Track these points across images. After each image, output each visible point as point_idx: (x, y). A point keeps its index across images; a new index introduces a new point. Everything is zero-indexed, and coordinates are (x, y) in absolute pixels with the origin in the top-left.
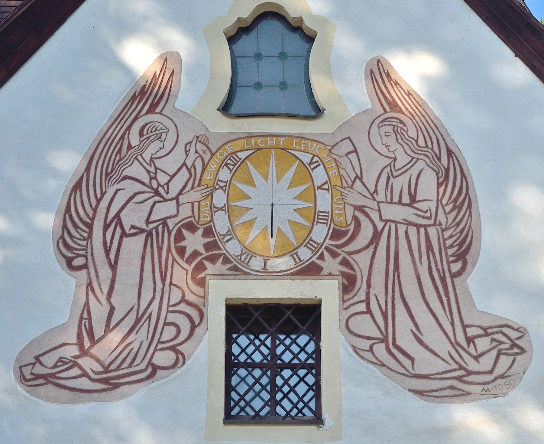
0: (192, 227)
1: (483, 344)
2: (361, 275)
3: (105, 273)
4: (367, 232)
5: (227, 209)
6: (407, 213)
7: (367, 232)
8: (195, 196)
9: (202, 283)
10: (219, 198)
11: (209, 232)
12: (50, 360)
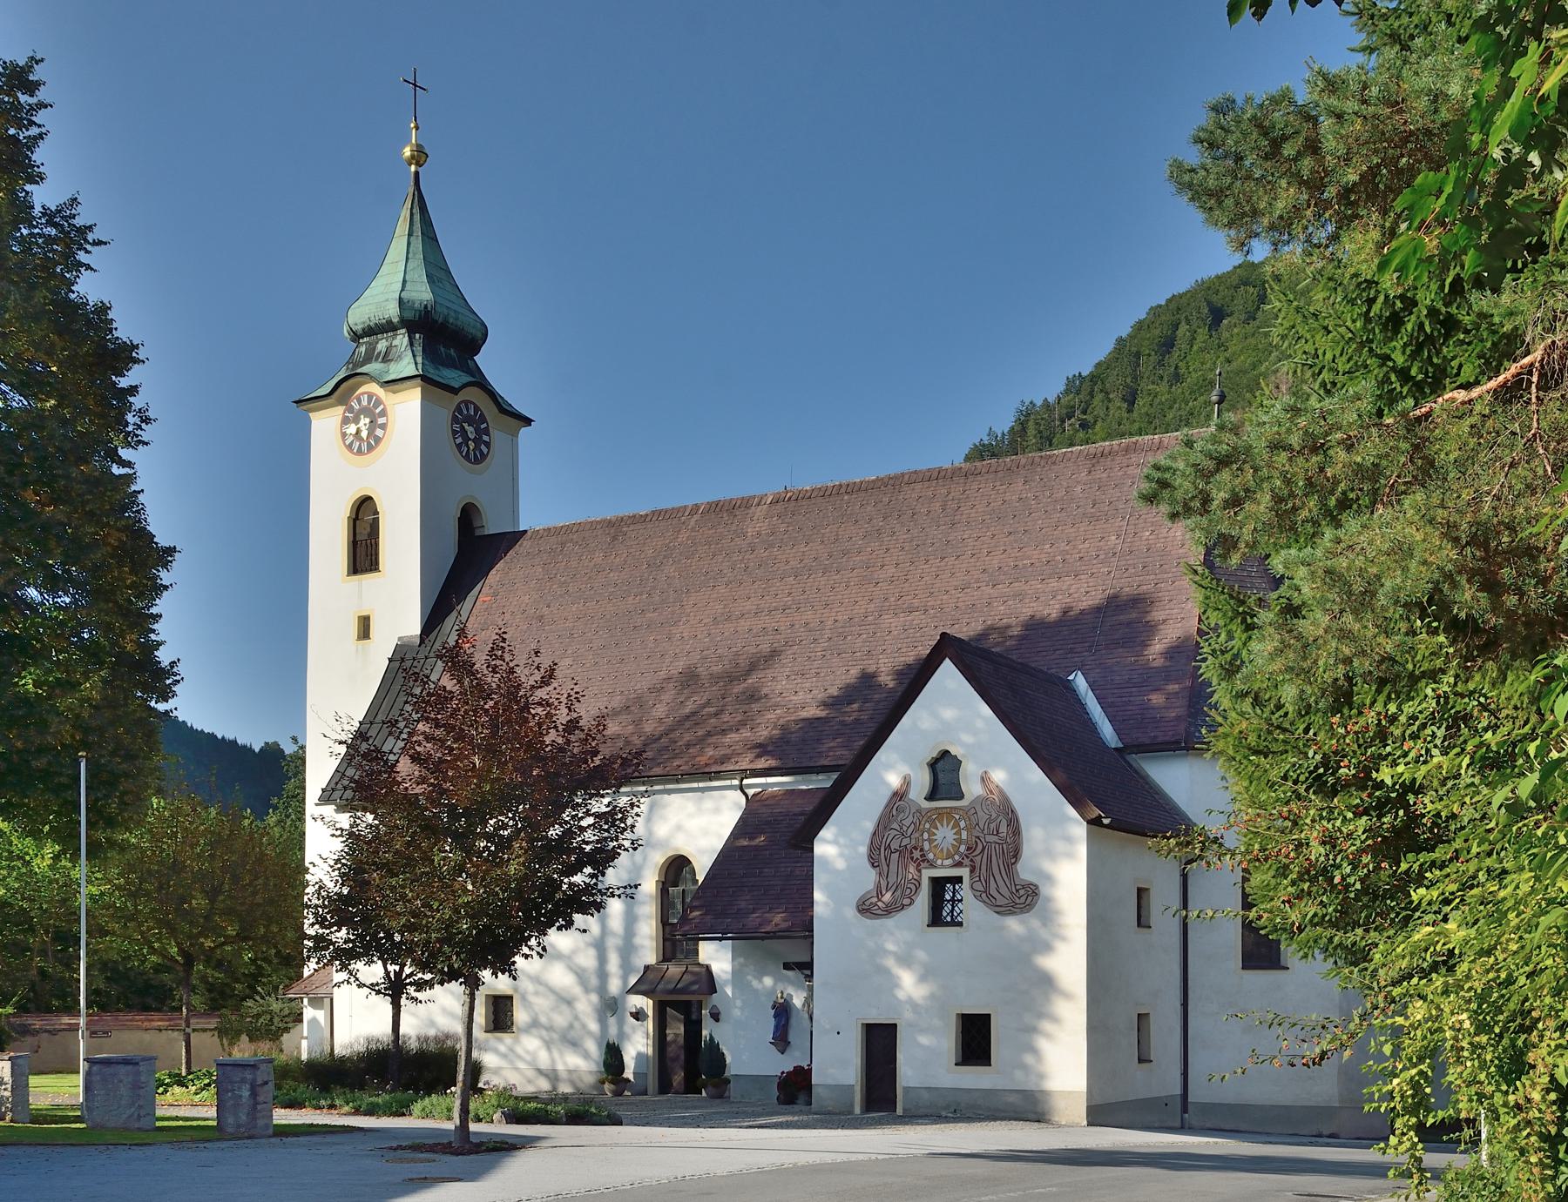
0: (916, 849)
1: (1022, 892)
2: (977, 866)
3: (885, 868)
4: (980, 847)
5: (930, 841)
6: (995, 838)
7: (980, 847)
8: (917, 835)
9: (919, 871)
10: (926, 836)
11: (922, 850)
12: (867, 903)
